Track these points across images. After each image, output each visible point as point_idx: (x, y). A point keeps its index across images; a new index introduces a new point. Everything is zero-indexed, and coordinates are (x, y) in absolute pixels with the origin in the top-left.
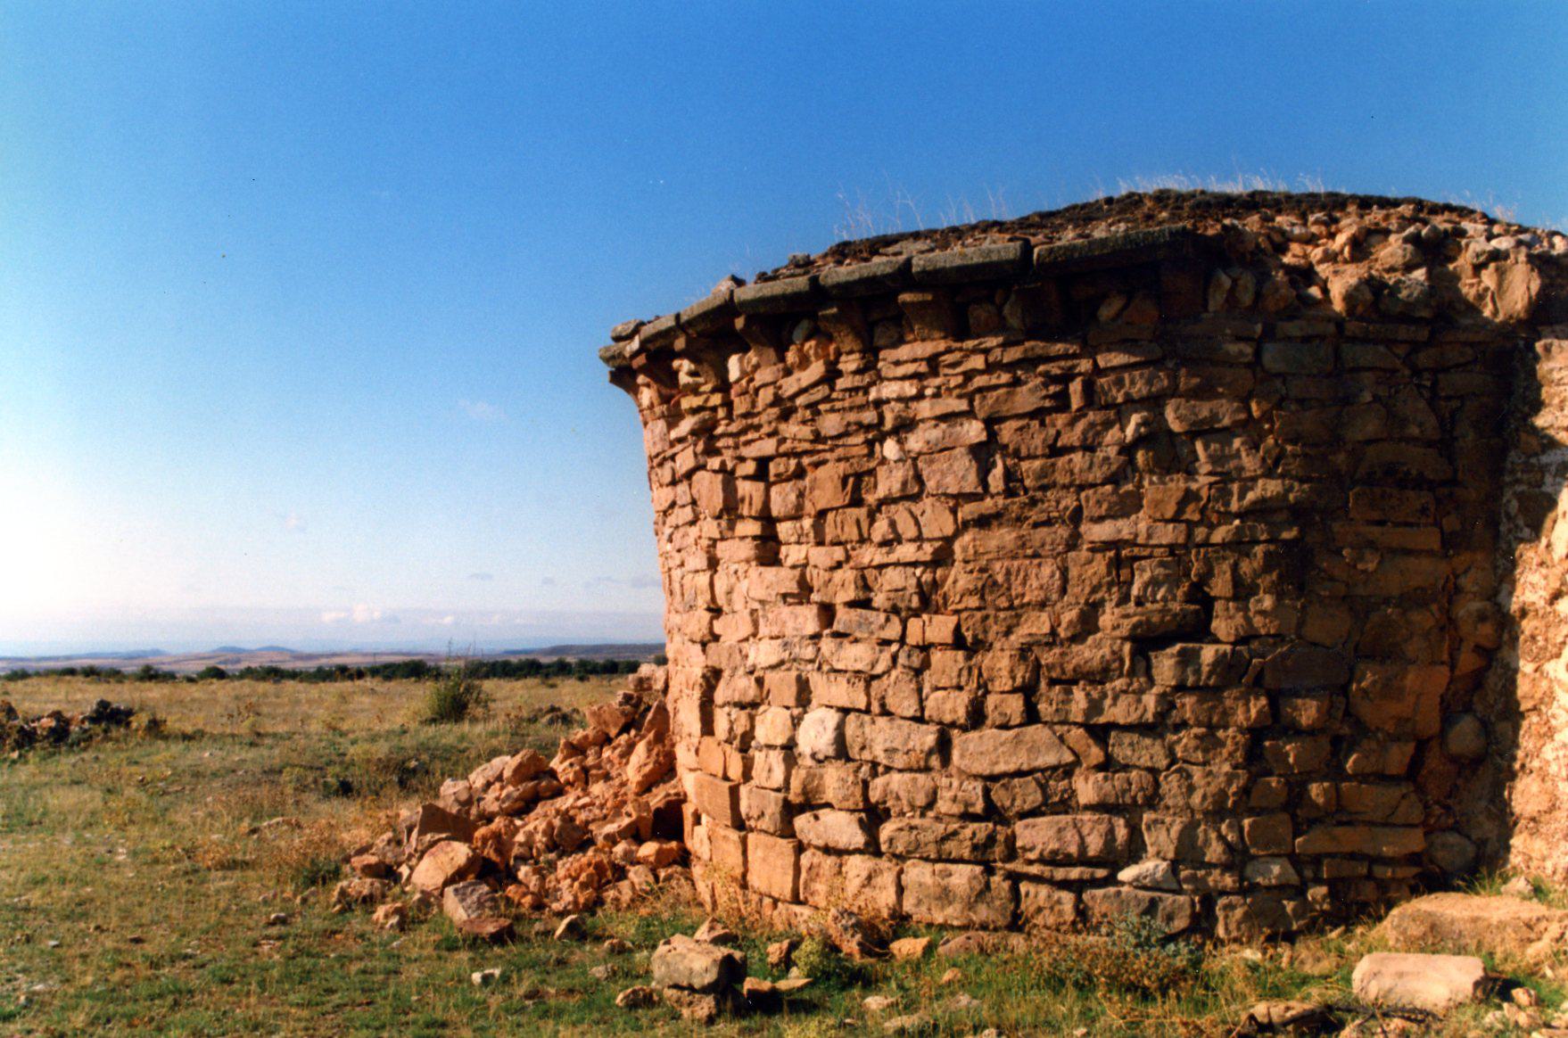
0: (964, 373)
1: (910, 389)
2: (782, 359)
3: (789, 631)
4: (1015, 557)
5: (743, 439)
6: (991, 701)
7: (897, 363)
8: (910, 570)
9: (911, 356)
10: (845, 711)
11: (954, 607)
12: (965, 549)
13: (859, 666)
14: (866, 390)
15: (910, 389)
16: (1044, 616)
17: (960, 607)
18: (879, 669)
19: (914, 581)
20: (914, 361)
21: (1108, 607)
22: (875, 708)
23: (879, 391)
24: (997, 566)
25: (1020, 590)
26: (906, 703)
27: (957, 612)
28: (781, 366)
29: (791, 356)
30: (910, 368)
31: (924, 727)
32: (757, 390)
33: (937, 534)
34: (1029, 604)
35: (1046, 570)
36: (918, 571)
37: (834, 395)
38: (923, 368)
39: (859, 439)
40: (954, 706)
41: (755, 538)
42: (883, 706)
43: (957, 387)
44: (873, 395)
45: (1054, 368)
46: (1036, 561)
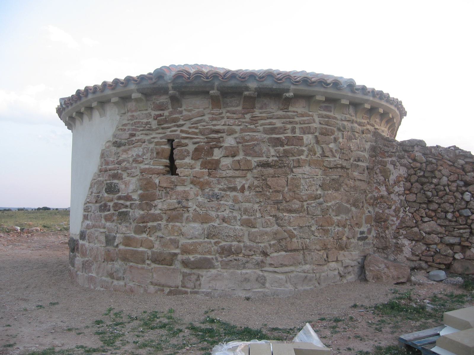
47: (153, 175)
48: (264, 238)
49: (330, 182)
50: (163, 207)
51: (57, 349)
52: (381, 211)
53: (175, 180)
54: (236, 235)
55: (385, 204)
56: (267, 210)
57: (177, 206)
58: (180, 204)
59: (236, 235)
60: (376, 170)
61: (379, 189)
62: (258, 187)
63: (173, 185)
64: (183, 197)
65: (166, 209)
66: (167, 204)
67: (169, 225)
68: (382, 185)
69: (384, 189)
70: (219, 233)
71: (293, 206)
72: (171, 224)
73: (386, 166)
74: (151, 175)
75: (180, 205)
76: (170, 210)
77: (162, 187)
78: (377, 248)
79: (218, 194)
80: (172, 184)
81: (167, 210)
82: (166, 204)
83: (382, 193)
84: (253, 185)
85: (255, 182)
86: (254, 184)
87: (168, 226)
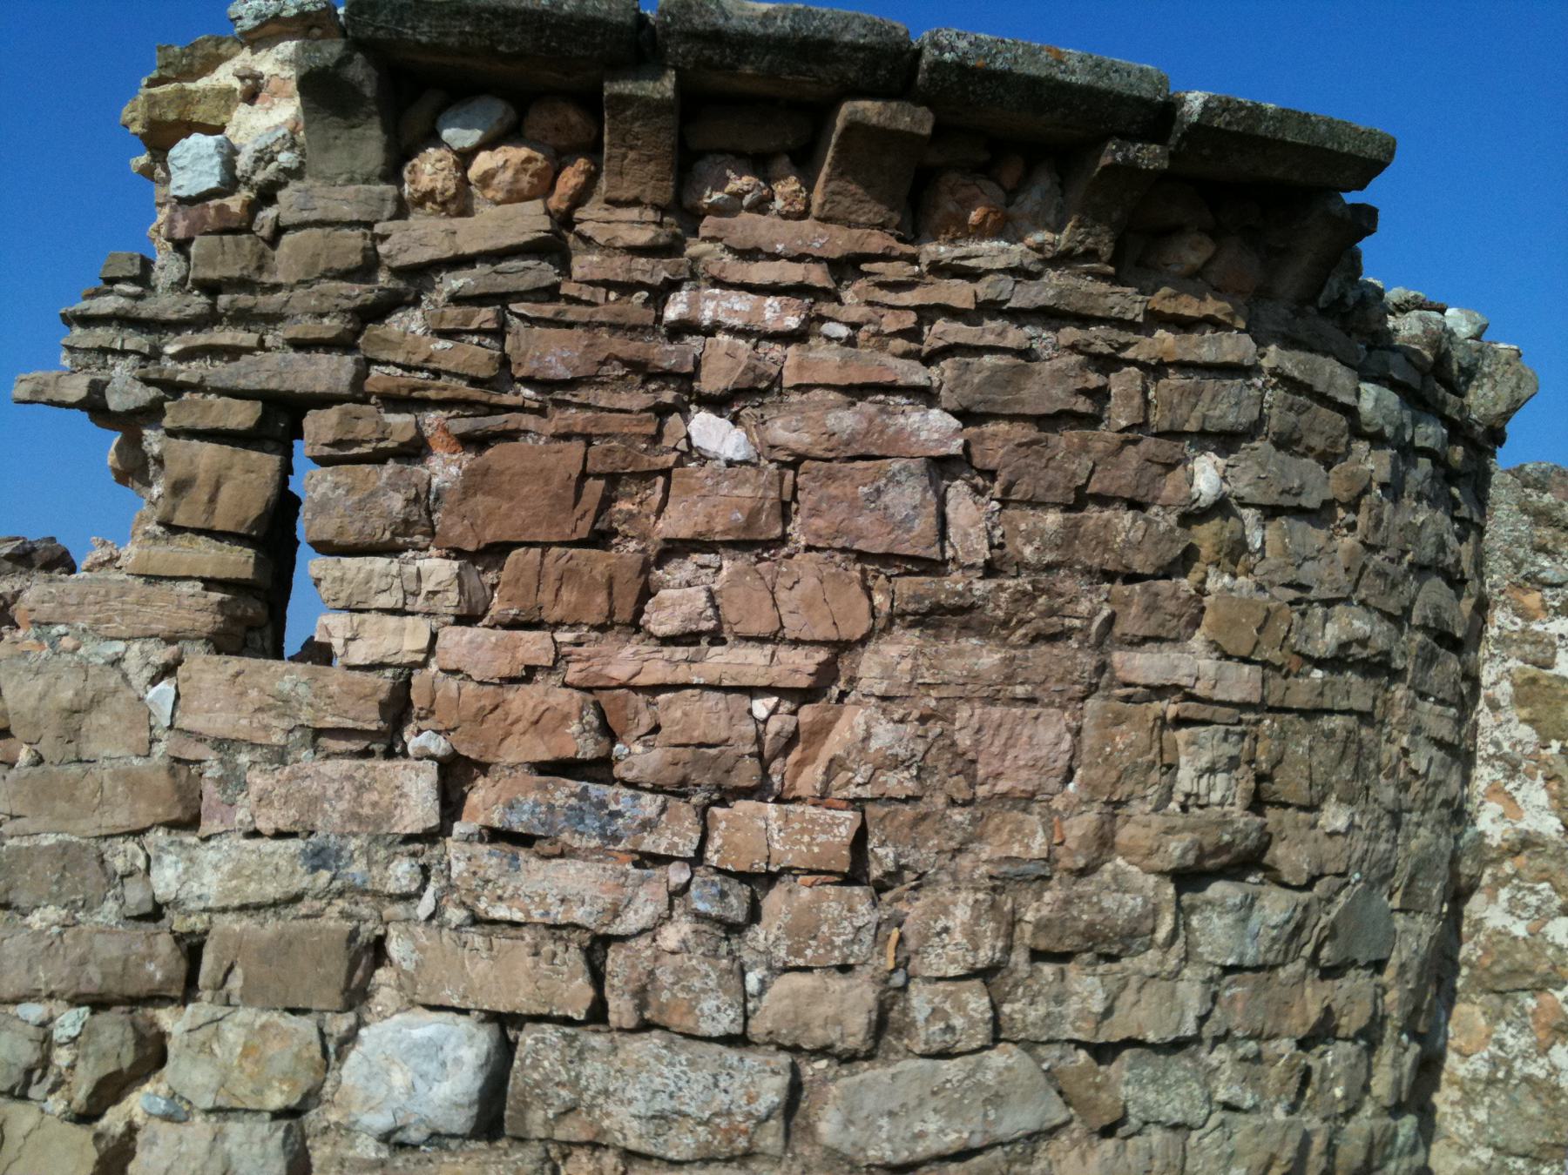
0: (918, 309)
1: (778, 314)
2: (392, 174)
3: (330, 820)
4: (992, 700)
5: (558, 395)
6: (920, 1001)
7: (750, 254)
8: (742, 701)
9: (799, 246)
10: (505, 1023)
11: (853, 792)
12: (888, 672)
13: (579, 915)
14: (660, 294)
15: (778, 314)
16: (1034, 820)
17: (866, 793)
18: (631, 922)
19: (749, 729)
20: (799, 258)
21: (1137, 808)
22: (621, 1008)
23: (693, 304)
24: (963, 712)
25: (996, 765)
26: (708, 1005)
27: (856, 803)
28: (389, 190)
29: (430, 170)
30: (793, 273)
31: (752, 1060)
32: (279, 230)
33: (823, 631)
34: (1003, 796)
35: (1046, 734)
36: (761, 707)
37: (567, 289)
38: (817, 276)
39: (637, 400)
40: (846, 1007)
41: (1459, 655)
42: (642, 996)
43: (901, 334)
44: (674, 311)
45: (1099, 338)
46: (1034, 711)
47: (136, 647)
48: (917, 1127)
49: (1311, 749)
50: (195, 888)
51: (296, 443)
52: (1520, 930)
53: (302, 689)
54: (729, 1113)
55: (1546, 885)
56: (946, 930)
57: (302, 881)
58: (325, 866)
59: (729, 1113)
60: (1495, 684)
61: (1513, 799)
62: (896, 763)
63: (286, 723)
64: (355, 816)
65: (211, 904)
66: (227, 868)
67: (225, 1026)
68: (1532, 776)
69: (1542, 797)
70: (606, 1092)
71: (1109, 902)
72: (244, 1014)
73: (1549, 666)
74: (119, 647)
75: (324, 876)
76: (243, 908)
77: (200, 738)
78: (1497, 1149)
79: (613, 807)
80: (282, 716)
81: (224, 910)
82: (216, 867)
83: (1529, 823)
84: (863, 750)
85: (875, 730)
86: (874, 745)
87: (217, 1035)
